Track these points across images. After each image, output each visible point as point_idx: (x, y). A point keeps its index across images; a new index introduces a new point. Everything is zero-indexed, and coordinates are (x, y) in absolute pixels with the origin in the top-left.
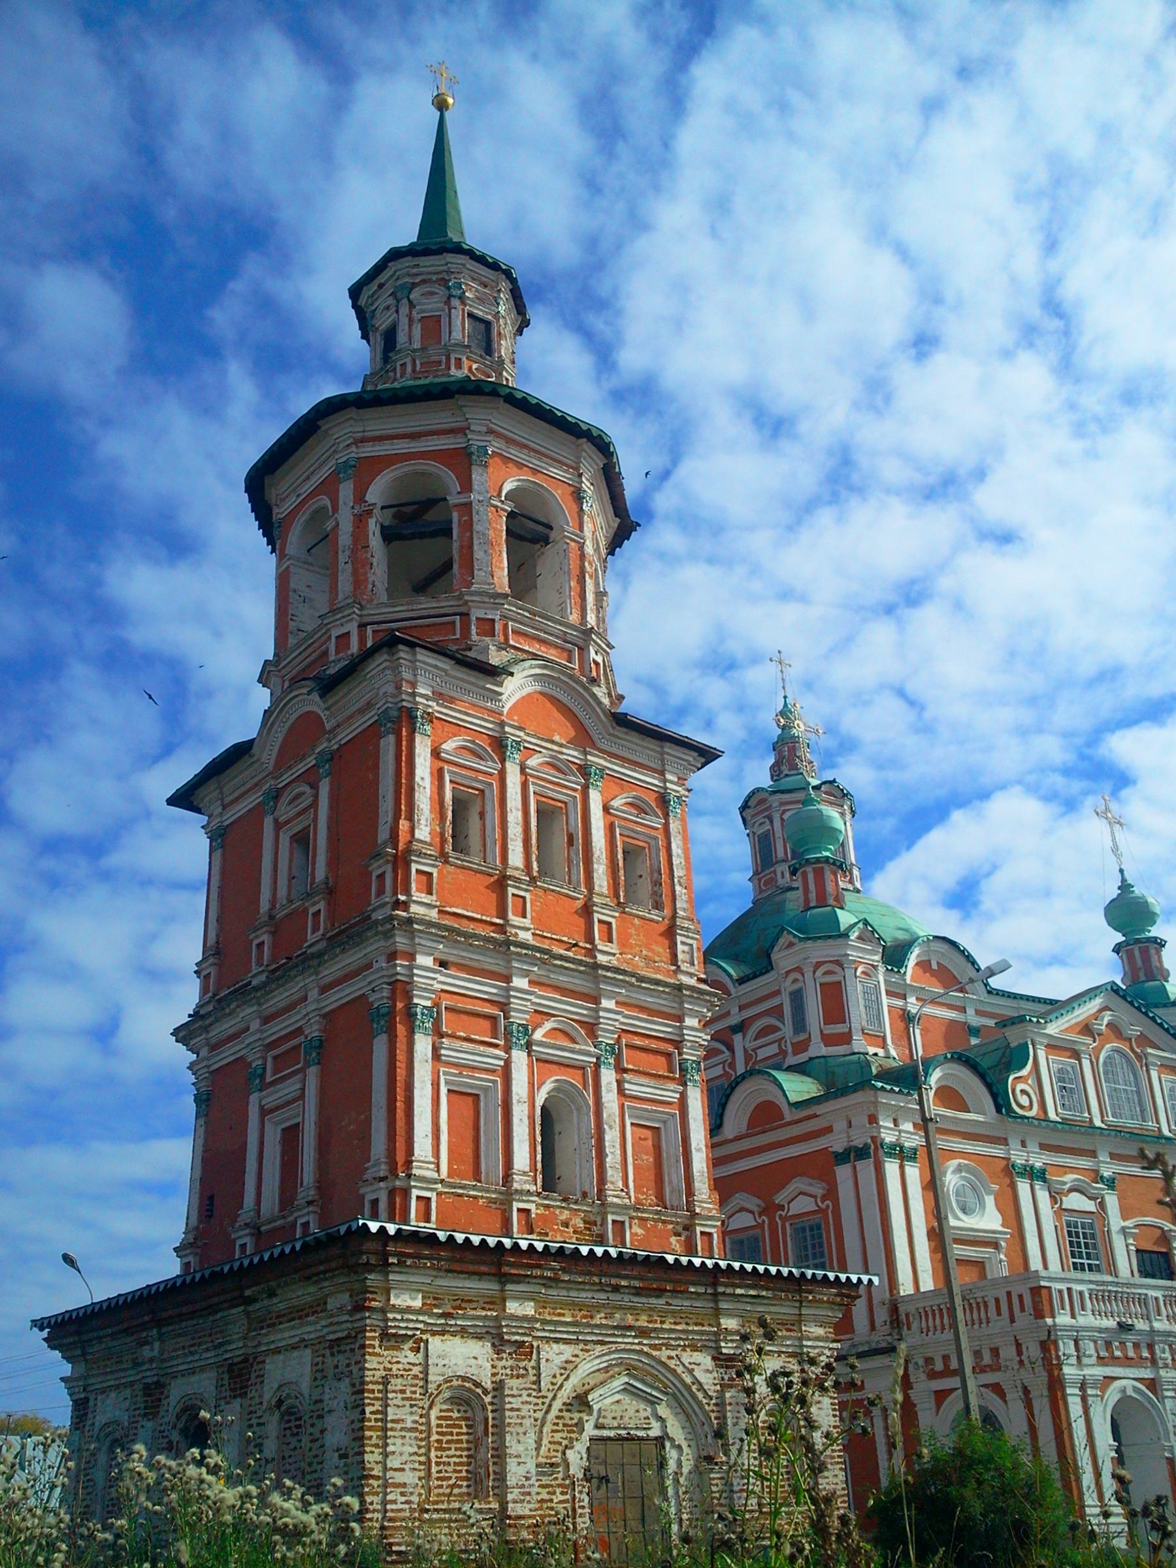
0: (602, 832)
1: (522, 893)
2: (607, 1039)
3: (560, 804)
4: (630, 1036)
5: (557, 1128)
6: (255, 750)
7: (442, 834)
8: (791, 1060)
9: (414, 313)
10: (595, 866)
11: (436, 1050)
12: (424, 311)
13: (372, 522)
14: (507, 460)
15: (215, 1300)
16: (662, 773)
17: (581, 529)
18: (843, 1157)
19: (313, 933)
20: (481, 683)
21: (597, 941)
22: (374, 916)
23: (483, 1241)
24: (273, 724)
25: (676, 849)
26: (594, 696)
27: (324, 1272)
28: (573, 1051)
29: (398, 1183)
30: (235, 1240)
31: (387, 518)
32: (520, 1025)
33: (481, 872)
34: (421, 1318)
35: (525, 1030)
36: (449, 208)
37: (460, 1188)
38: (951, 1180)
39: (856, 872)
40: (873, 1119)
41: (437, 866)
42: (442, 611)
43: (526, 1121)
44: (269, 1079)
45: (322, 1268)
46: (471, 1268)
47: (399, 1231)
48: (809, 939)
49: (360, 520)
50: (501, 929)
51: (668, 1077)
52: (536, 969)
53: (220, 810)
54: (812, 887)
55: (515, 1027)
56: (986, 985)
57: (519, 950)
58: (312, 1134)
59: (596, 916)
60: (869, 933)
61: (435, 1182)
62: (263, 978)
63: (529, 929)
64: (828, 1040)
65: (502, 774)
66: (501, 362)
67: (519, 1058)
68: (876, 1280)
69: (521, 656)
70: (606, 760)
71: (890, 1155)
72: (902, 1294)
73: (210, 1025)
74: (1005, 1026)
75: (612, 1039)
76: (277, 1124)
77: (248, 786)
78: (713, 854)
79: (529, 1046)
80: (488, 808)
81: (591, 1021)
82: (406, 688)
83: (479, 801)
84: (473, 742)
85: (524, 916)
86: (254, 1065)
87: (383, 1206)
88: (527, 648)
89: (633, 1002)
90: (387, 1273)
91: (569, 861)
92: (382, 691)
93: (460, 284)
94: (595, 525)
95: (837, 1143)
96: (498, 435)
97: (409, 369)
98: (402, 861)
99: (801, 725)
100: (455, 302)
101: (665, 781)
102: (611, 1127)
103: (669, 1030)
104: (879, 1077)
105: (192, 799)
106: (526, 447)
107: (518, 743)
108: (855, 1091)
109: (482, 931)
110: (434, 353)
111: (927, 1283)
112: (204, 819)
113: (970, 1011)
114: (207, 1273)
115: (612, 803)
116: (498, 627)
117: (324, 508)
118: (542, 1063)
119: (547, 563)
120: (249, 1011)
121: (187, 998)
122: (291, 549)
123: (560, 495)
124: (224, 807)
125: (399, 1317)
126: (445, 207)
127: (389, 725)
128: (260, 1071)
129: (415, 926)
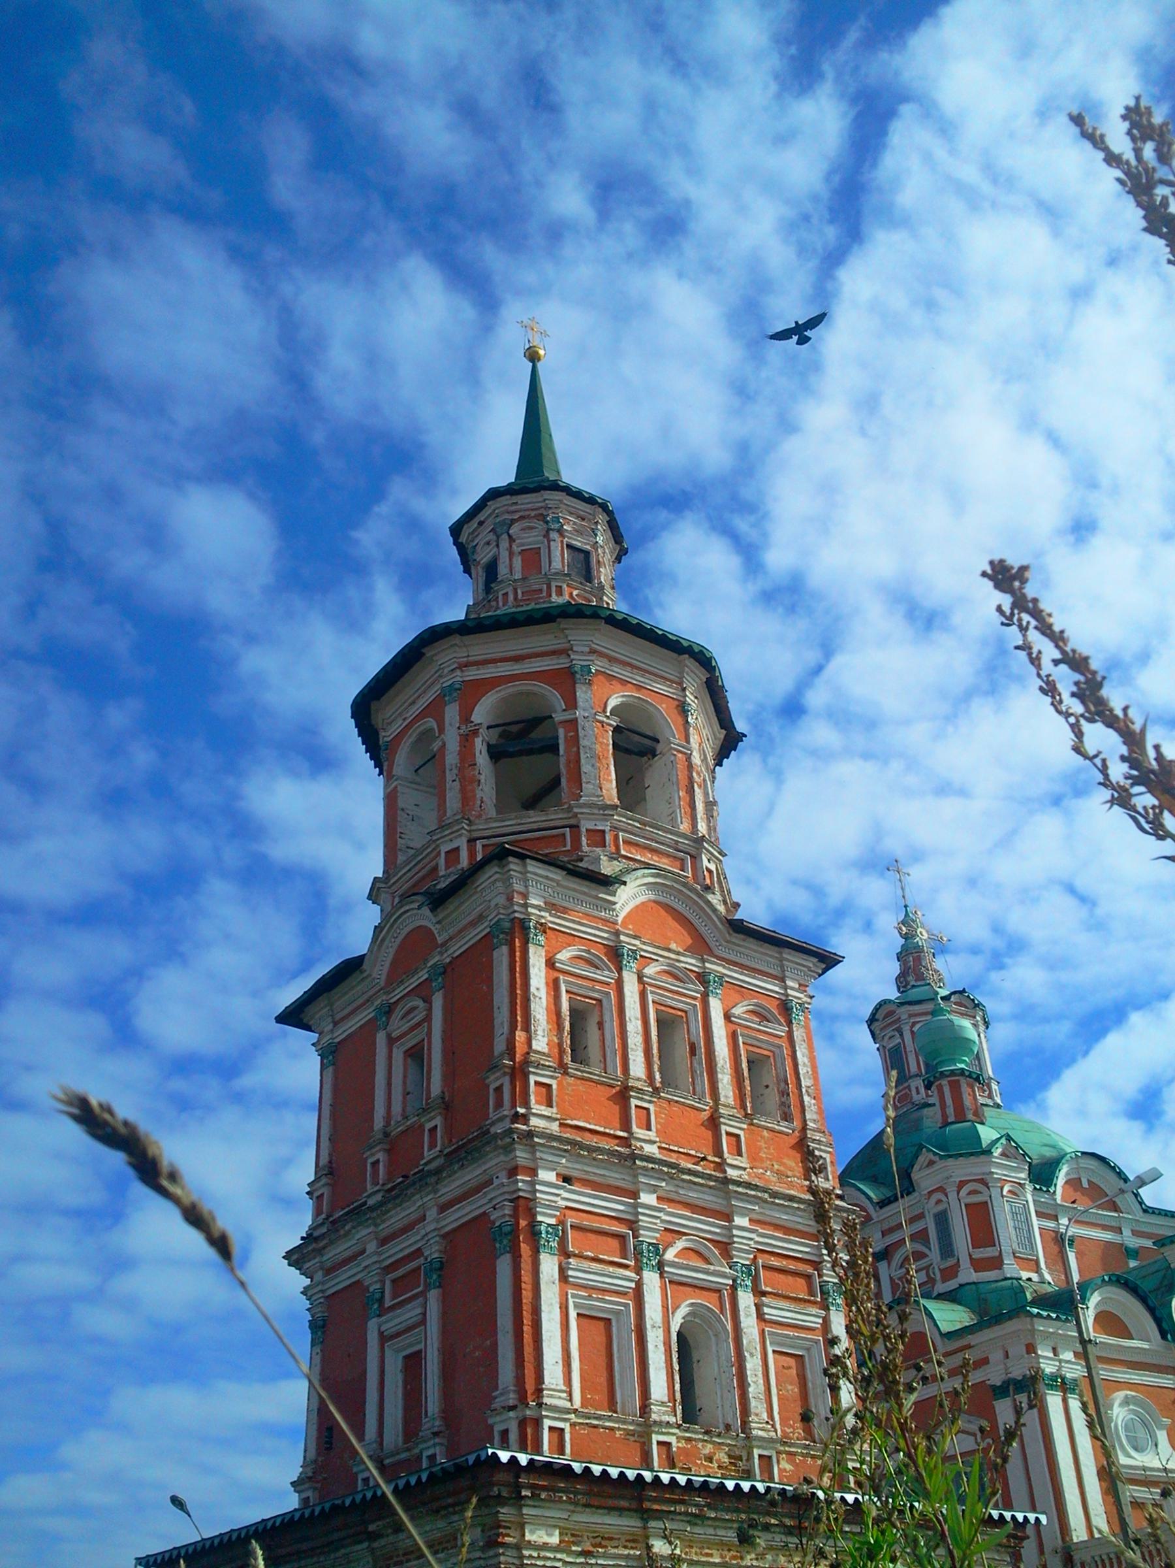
0: (725, 1041)
1: (645, 1105)
2: (743, 1259)
3: (680, 1013)
4: (766, 1256)
5: (695, 1356)
6: (366, 965)
7: (560, 1045)
8: (941, 1287)
9: (514, 546)
10: (720, 1076)
11: (562, 1271)
12: (522, 545)
13: (478, 742)
14: (611, 678)
15: (336, 1536)
16: (782, 980)
17: (688, 741)
18: (1002, 1390)
19: (429, 1150)
20: (594, 893)
21: (726, 1155)
22: (493, 1130)
23: (622, 1473)
24: (383, 940)
25: (802, 1058)
26: (708, 903)
27: (453, 1505)
28: (707, 1272)
29: (528, 1412)
30: (356, 1474)
31: (493, 736)
32: (650, 1244)
33: (603, 1083)
34: (559, 1556)
35: (656, 1249)
36: (544, 450)
37: (595, 1418)
38: (1119, 1414)
39: (994, 1086)
40: (1031, 1349)
41: (555, 1078)
42: (552, 824)
43: (662, 1348)
44: (388, 1303)
45: (450, 1501)
46: (610, 1502)
47: (531, 1461)
48: (950, 1156)
49: (467, 740)
50: (625, 1141)
51: (809, 1301)
52: (663, 1184)
53: (331, 1026)
54: (949, 1101)
55: (644, 1246)
56: (1137, 1195)
57: (645, 1164)
58: (436, 1361)
59: (724, 1128)
60: (1014, 1150)
61: (568, 1411)
62: (379, 1197)
63: (655, 1142)
64: (978, 1265)
65: (619, 984)
66: (601, 587)
67: (651, 1279)
68: (1043, 1519)
69: (632, 865)
70: (724, 967)
71: (1051, 1387)
72: (1075, 1540)
73: (324, 1248)
74: (1163, 1245)
75: (748, 1259)
76: (398, 1351)
77: (361, 1001)
78: (844, 1077)
79: (660, 1266)
80: (607, 1018)
81: (725, 1240)
82: (518, 899)
83: (596, 1013)
84: (588, 952)
85: (649, 1129)
86: (371, 1289)
87: (513, 1436)
88: (639, 858)
89: (768, 1219)
90: (520, 1507)
91: (693, 1071)
92: (493, 904)
93: (558, 518)
94: (701, 737)
95: (994, 1375)
96: (601, 655)
97: (511, 597)
98: (520, 1073)
99: (924, 933)
100: (554, 535)
101: (786, 988)
102: (752, 1355)
103: (807, 1250)
104: (1034, 1303)
105: (302, 1016)
106: (630, 665)
107: (634, 952)
108: (1010, 1319)
109: (606, 1144)
110: (535, 582)
111: (1100, 1521)
112: (314, 1037)
113: (1126, 1232)
114: (327, 1506)
115: (733, 1011)
116: (609, 838)
117: (432, 729)
118: (676, 1285)
119: (655, 774)
120: (365, 1232)
121: (302, 1221)
122: (397, 770)
123: (666, 711)
124: (336, 1024)
125: (535, 1554)
126: (540, 449)
127: (501, 936)
128: (377, 1296)
129: (536, 1140)
